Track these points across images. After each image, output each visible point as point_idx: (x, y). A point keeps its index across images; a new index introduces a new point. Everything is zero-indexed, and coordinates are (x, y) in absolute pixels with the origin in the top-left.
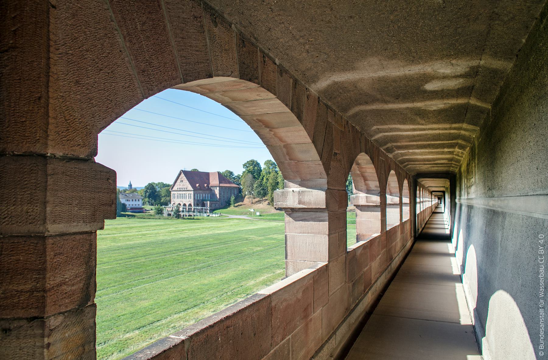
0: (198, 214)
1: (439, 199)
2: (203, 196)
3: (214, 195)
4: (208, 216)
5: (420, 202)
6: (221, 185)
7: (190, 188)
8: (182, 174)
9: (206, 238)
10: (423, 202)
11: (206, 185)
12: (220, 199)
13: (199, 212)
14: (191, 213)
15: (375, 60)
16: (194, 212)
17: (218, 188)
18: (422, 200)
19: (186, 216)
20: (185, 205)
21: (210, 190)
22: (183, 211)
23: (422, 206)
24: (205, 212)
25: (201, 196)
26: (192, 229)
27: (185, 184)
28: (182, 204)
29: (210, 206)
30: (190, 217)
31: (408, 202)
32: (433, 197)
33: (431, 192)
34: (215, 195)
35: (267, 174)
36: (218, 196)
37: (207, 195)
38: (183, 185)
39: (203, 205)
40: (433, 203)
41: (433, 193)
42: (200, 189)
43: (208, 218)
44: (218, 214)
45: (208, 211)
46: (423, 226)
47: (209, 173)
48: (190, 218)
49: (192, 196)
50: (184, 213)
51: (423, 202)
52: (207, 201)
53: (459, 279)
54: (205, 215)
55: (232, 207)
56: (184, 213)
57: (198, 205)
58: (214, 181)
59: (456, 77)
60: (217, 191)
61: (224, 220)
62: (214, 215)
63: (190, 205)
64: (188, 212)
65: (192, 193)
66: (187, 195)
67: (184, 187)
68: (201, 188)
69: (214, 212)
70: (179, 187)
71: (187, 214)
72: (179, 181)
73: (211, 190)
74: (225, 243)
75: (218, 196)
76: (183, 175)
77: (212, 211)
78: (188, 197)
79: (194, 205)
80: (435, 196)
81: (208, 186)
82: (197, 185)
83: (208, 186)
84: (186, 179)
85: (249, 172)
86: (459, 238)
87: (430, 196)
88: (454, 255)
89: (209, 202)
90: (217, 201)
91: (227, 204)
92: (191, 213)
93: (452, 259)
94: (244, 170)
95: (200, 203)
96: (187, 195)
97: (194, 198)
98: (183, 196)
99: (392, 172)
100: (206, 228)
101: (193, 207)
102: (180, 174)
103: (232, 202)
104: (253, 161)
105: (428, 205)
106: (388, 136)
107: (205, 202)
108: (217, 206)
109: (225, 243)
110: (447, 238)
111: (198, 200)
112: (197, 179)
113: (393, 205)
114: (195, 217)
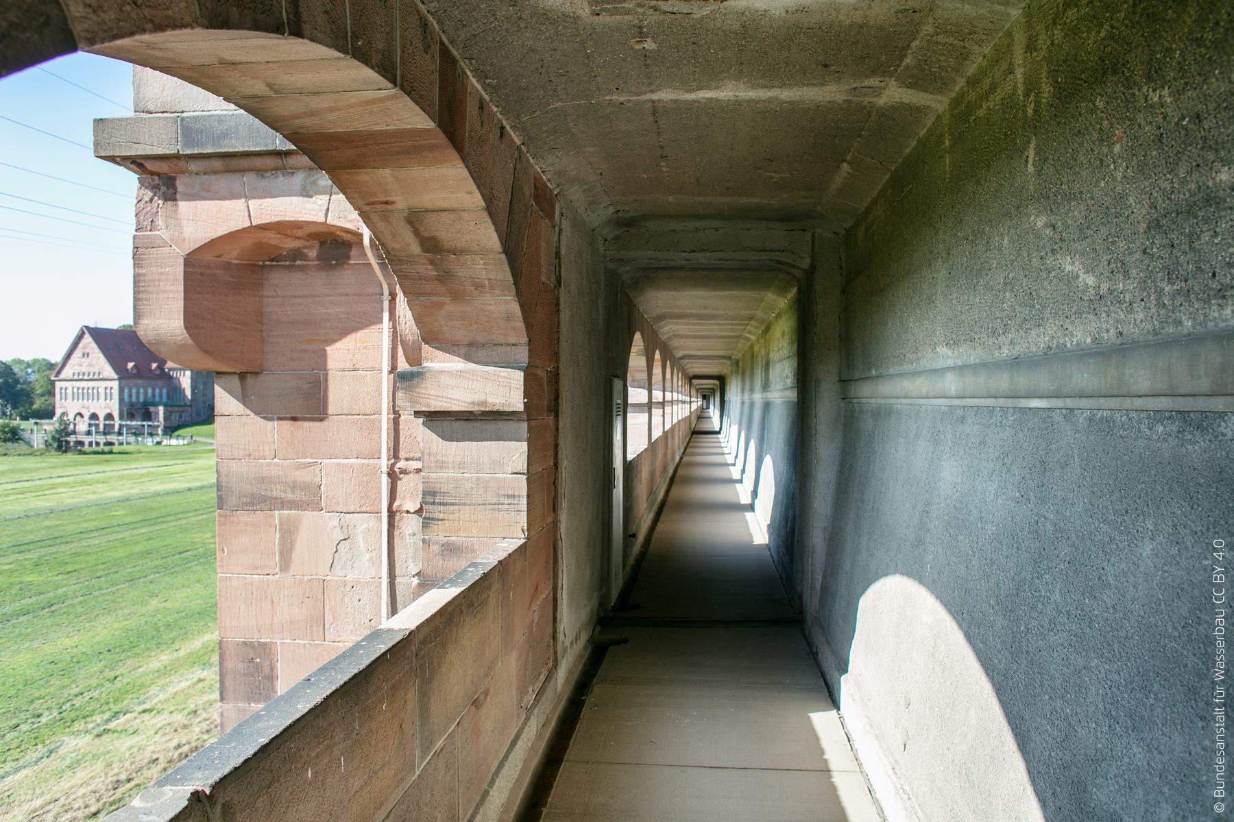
0: (132, 439)
1: (704, 397)
2: (146, 393)
3: (176, 390)
4: (159, 443)
5: (649, 406)
7: (109, 371)
8: (87, 336)
9: (104, 507)
10: (672, 402)
11: (154, 365)
12: (193, 400)
13: (135, 434)
14: (111, 438)
16: (120, 434)
18: (657, 395)
19: (98, 444)
20: (94, 416)
22: (89, 433)
23: (668, 417)
24: (151, 435)
25: (141, 392)
26: (85, 483)
27: (98, 362)
28: (87, 415)
29: (165, 419)
30: (107, 449)
32: (694, 393)
33: (691, 378)
34: (182, 391)
36: (188, 393)
37: (160, 392)
38: (90, 365)
39: (147, 416)
40: (694, 406)
41: (695, 382)
43: (158, 447)
44: (184, 438)
45: (160, 432)
46: (661, 496)
48: (107, 451)
49: (116, 393)
50: (93, 438)
51: (663, 404)
52: (156, 405)
53: (751, 507)
54: (149, 441)
56: (93, 438)
57: (131, 416)
61: (198, 452)
62: (174, 442)
63: (109, 417)
64: (105, 434)
65: (115, 385)
66: (102, 391)
67: (92, 370)
68: (141, 373)
69: (177, 433)
71: (101, 439)
72: (77, 354)
73: (171, 378)
74: (155, 522)
75: (188, 393)
76: (88, 339)
77: (170, 430)
78: (102, 396)
79: (121, 417)
80: (697, 391)
82: (130, 365)
83: (161, 367)
84: (97, 350)
87: (687, 387)
88: (751, 507)
89: (161, 409)
90: (186, 405)
92: (111, 438)
93: (749, 515)
95: (137, 411)
96: (102, 391)
97: (121, 400)
98: (88, 393)
100: (131, 478)
101: (117, 422)
102: (80, 337)
105: (662, 422)
107: (152, 409)
108: (186, 417)
109: (155, 522)
111: (132, 405)
113: (638, 406)
114: (125, 448)
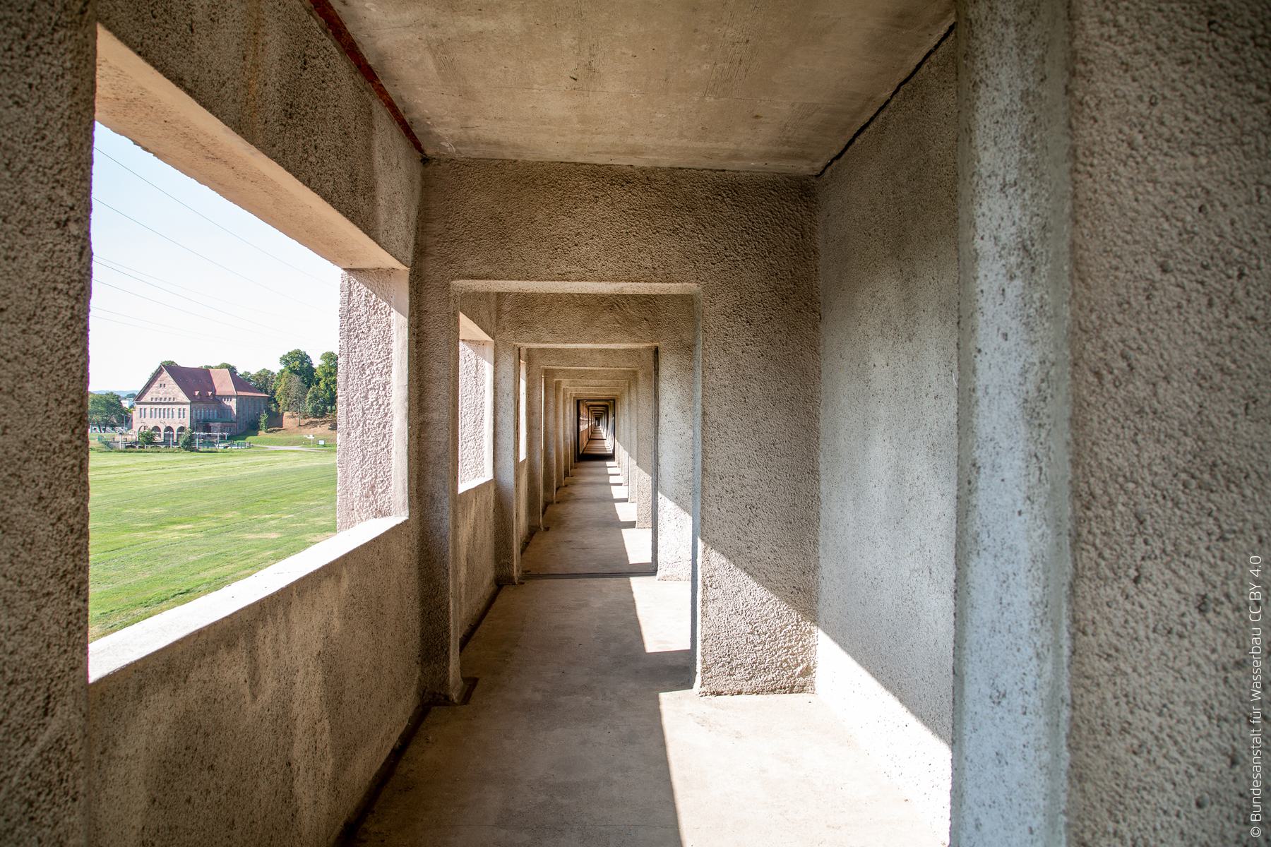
6: (240, 393)
7: (182, 397)
15: (618, 336)
17: (234, 400)
21: (217, 400)
25: (203, 412)
27: (172, 389)
28: (163, 429)
31: (111, 473)
35: (326, 376)
39: (207, 429)
42: (201, 401)
47: (208, 367)
55: (262, 433)
58: (224, 386)
59: (592, 484)
60: (232, 404)
63: (182, 429)
65: (188, 407)
70: (155, 396)
72: (157, 384)
76: (165, 374)
81: (214, 395)
83: (214, 395)
85: (293, 371)
86: (622, 454)
91: (253, 428)
94: (282, 367)
95: (202, 424)
99: (462, 317)
103: (262, 423)
104: (298, 352)
106: (589, 342)
110: (611, 457)
112: (194, 381)
